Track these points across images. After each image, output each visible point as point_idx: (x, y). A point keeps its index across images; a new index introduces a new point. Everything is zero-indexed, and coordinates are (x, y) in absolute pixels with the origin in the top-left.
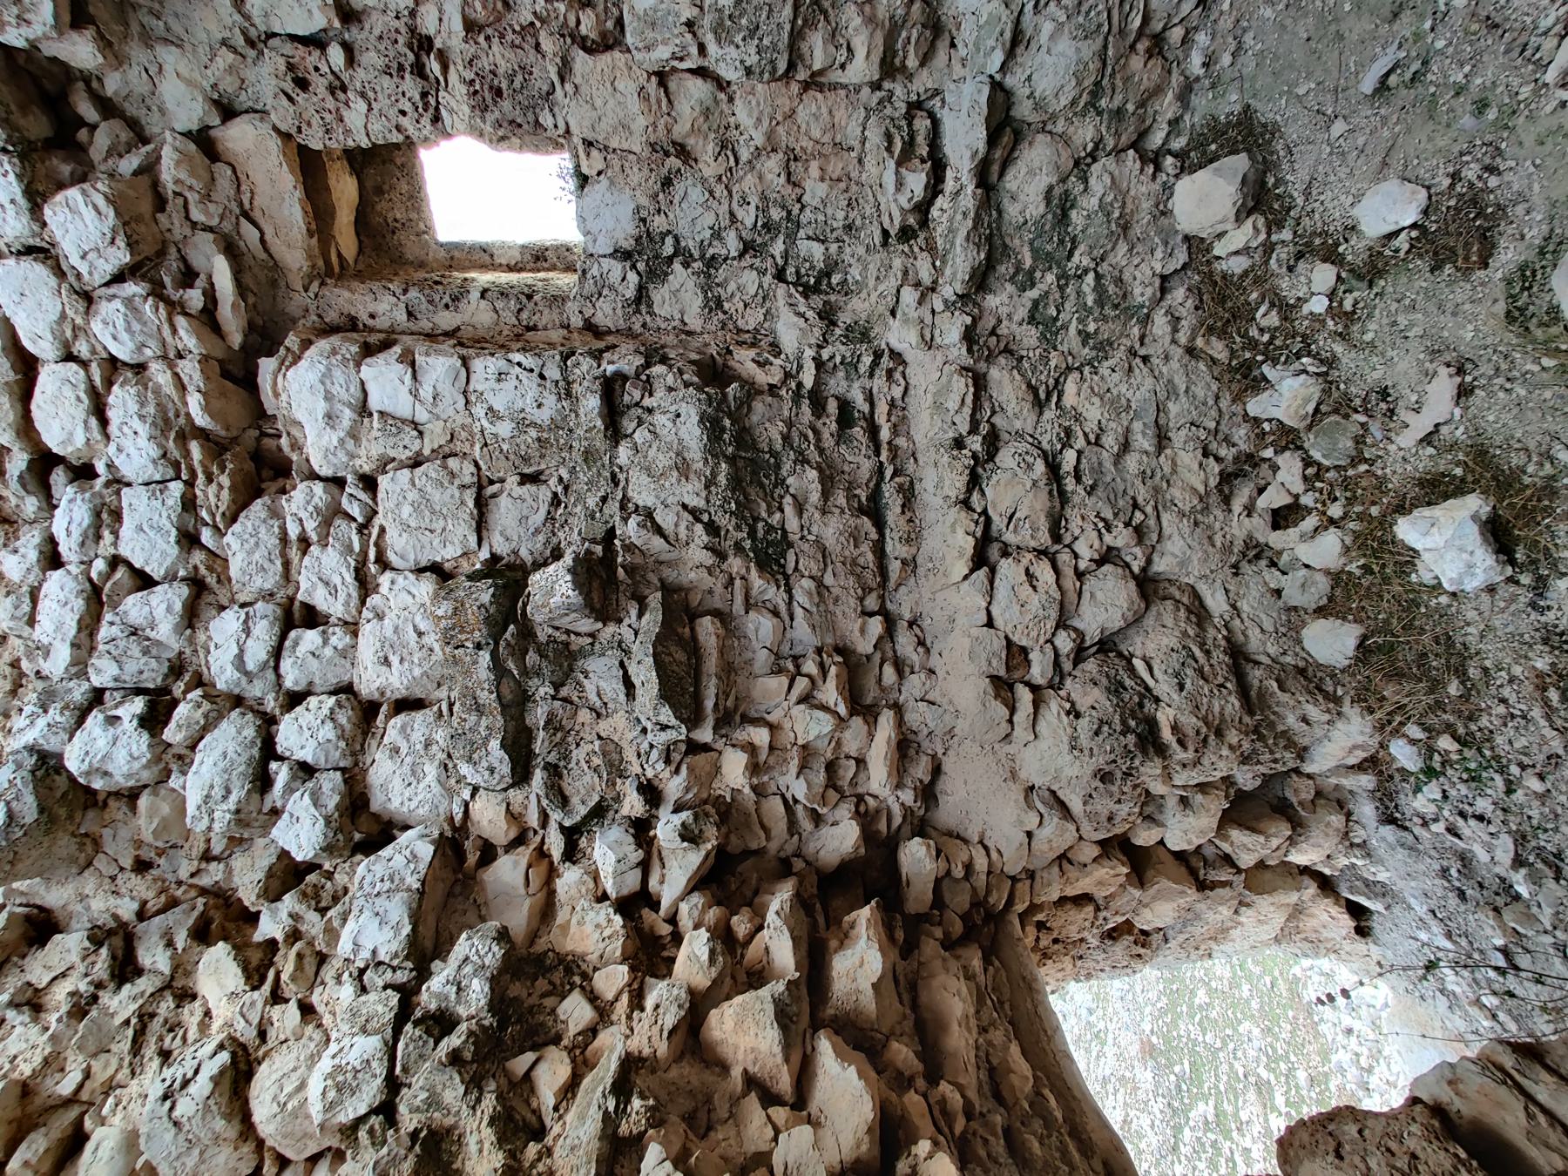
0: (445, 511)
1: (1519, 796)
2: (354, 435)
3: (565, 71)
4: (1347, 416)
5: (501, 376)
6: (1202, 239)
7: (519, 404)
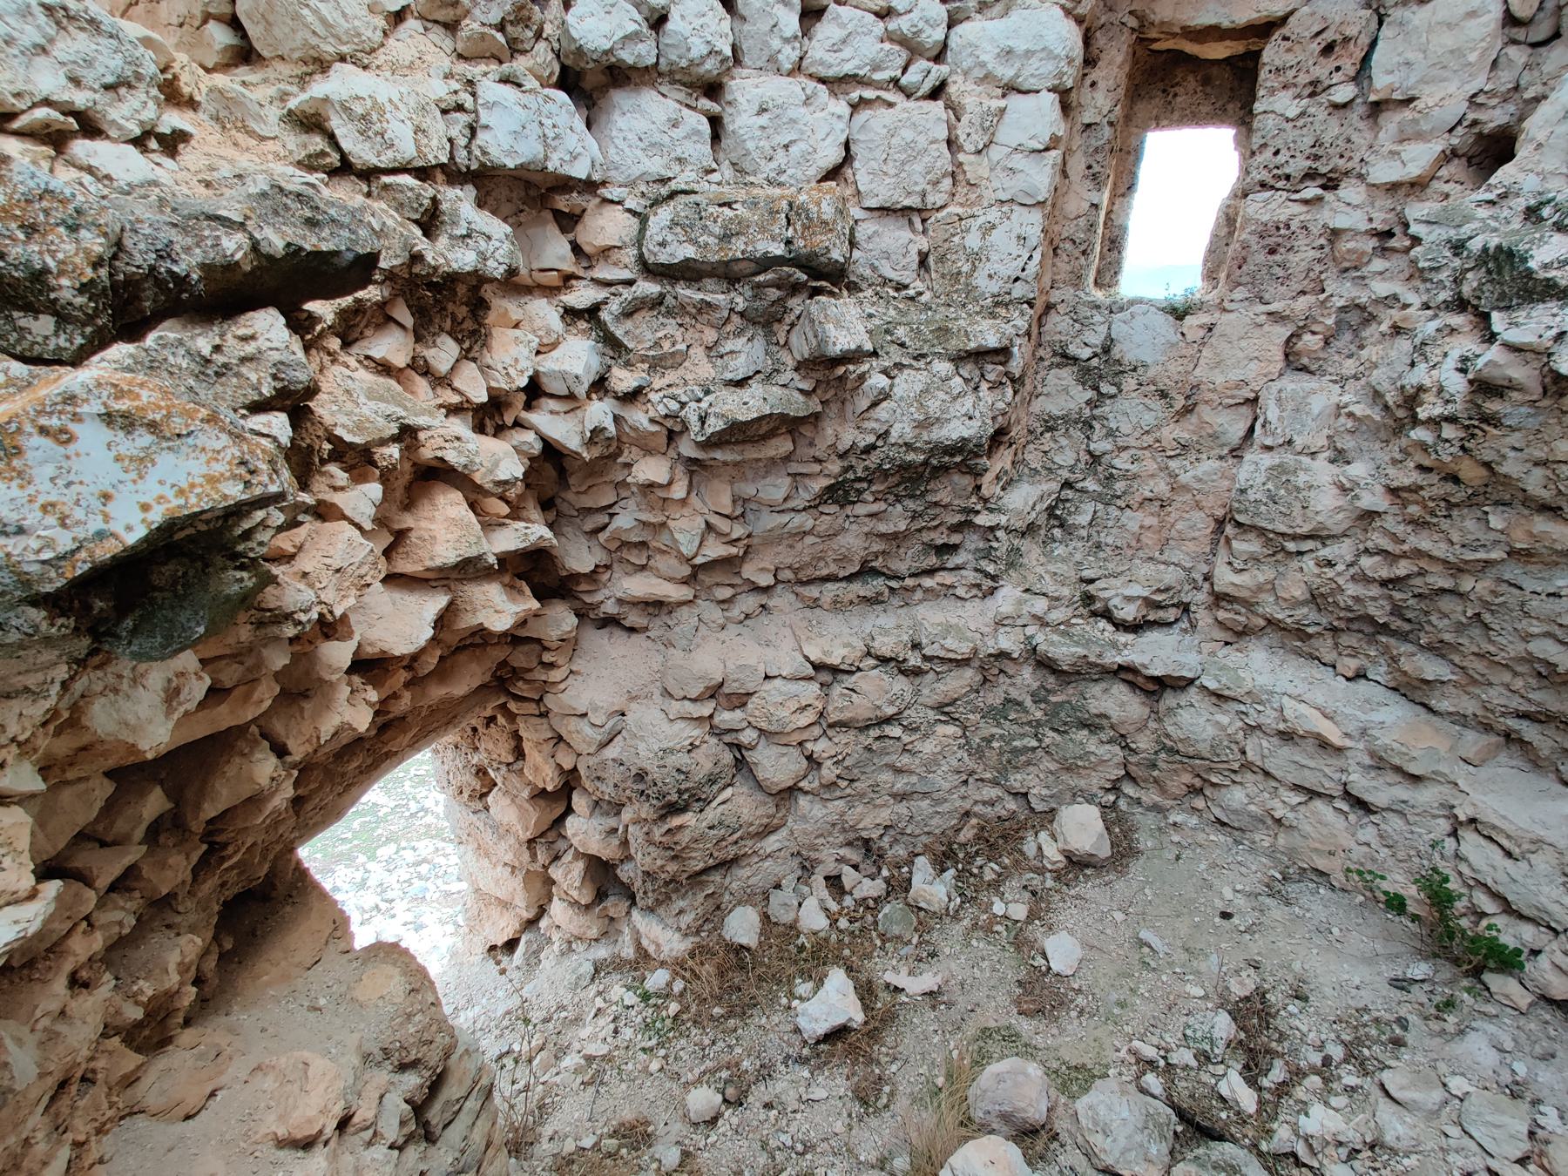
0: (903, 175)
1: (642, 1056)
2: (987, 78)
3: (1277, 317)
4: (916, 930)
5: (1022, 239)
6: (1052, 822)
7: (994, 257)
